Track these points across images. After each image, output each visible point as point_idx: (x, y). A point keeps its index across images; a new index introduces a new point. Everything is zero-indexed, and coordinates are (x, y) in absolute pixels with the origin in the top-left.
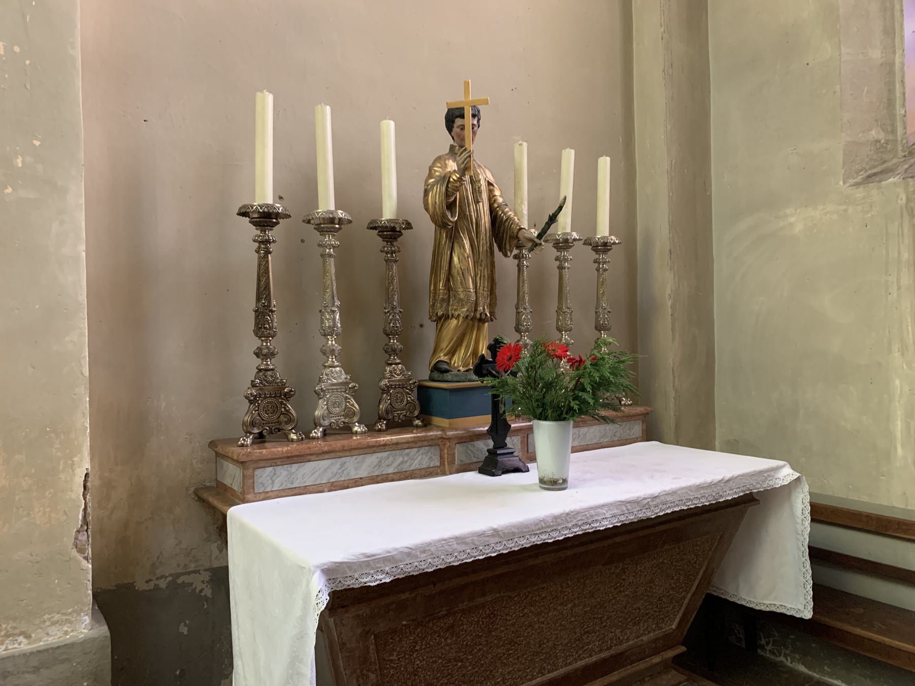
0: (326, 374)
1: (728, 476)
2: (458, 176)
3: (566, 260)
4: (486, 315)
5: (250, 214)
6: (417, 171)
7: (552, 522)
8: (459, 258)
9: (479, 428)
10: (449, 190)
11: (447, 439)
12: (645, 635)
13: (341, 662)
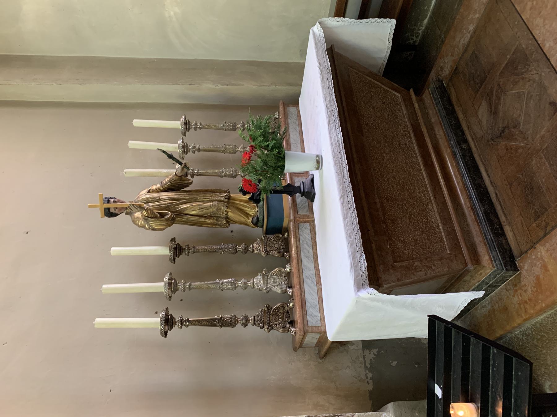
0: (258, 287)
1: (317, 64)
2: (144, 211)
3: (195, 147)
4: (226, 195)
5: (166, 330)
6: (140, 234)
7: (338, 166)
8: (193, 211)
9: (289, 201)
10: (152, 216)
11: (295, 219)
12: (403, 112)
13: (408, 281)
